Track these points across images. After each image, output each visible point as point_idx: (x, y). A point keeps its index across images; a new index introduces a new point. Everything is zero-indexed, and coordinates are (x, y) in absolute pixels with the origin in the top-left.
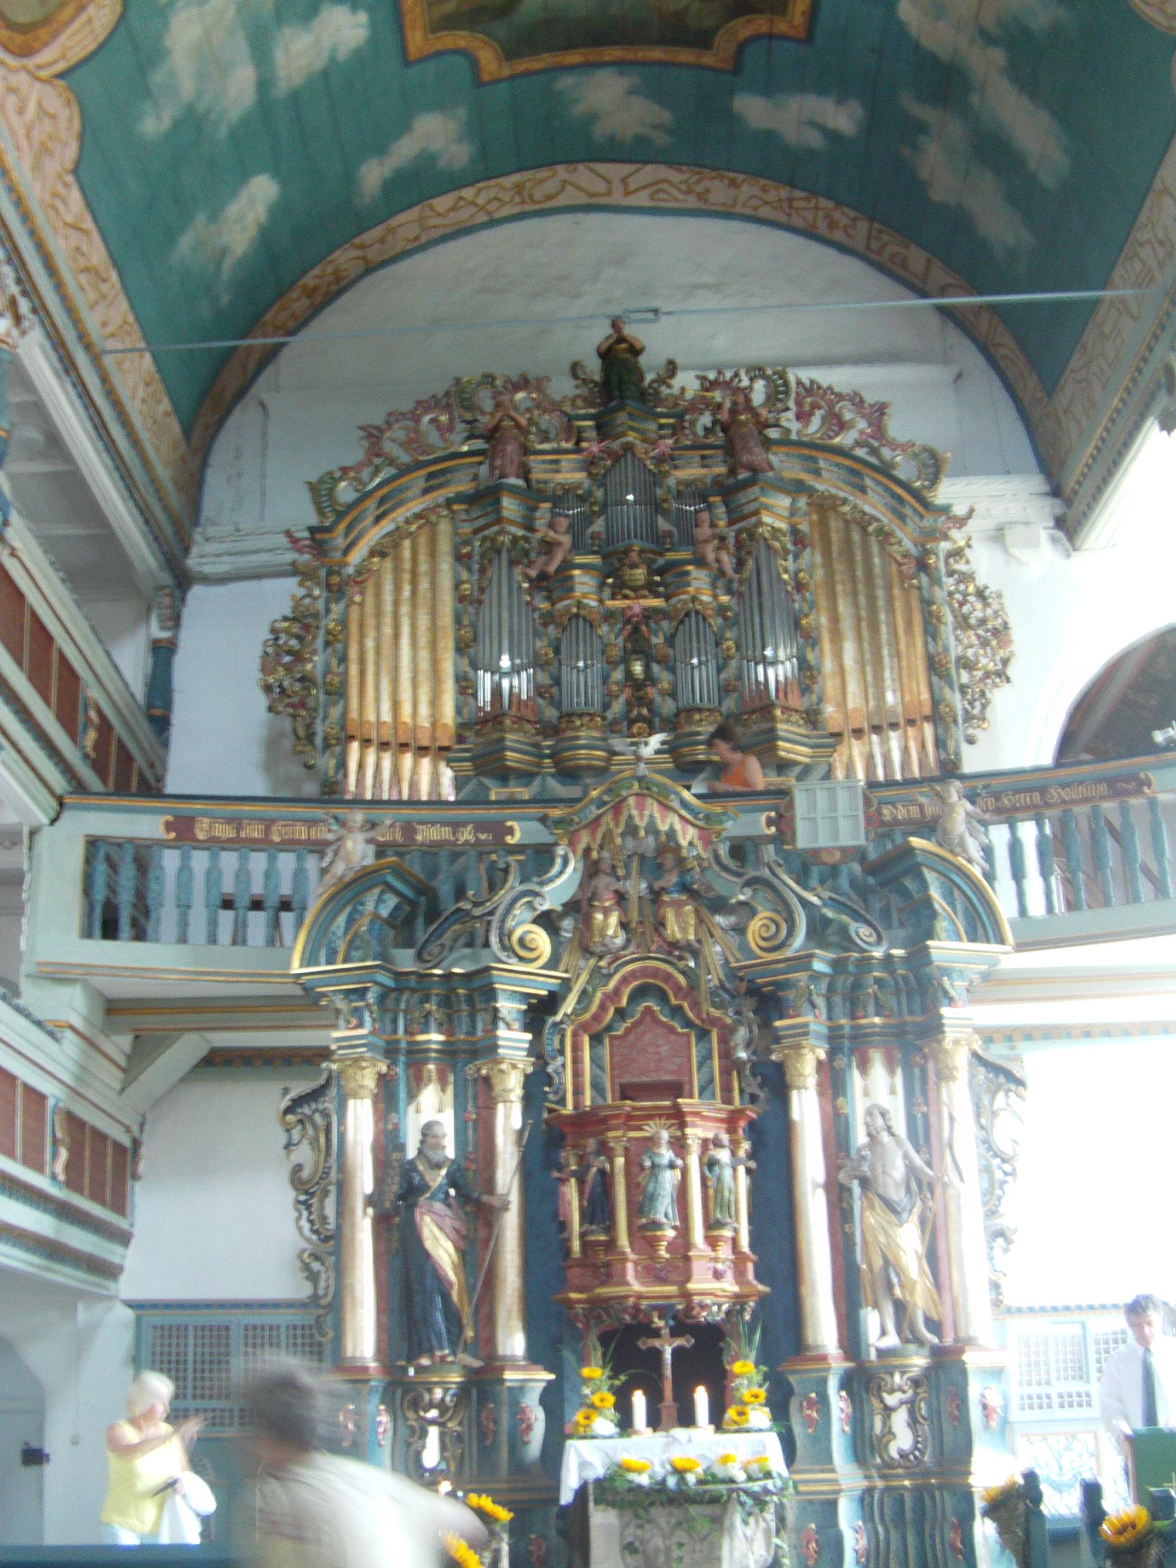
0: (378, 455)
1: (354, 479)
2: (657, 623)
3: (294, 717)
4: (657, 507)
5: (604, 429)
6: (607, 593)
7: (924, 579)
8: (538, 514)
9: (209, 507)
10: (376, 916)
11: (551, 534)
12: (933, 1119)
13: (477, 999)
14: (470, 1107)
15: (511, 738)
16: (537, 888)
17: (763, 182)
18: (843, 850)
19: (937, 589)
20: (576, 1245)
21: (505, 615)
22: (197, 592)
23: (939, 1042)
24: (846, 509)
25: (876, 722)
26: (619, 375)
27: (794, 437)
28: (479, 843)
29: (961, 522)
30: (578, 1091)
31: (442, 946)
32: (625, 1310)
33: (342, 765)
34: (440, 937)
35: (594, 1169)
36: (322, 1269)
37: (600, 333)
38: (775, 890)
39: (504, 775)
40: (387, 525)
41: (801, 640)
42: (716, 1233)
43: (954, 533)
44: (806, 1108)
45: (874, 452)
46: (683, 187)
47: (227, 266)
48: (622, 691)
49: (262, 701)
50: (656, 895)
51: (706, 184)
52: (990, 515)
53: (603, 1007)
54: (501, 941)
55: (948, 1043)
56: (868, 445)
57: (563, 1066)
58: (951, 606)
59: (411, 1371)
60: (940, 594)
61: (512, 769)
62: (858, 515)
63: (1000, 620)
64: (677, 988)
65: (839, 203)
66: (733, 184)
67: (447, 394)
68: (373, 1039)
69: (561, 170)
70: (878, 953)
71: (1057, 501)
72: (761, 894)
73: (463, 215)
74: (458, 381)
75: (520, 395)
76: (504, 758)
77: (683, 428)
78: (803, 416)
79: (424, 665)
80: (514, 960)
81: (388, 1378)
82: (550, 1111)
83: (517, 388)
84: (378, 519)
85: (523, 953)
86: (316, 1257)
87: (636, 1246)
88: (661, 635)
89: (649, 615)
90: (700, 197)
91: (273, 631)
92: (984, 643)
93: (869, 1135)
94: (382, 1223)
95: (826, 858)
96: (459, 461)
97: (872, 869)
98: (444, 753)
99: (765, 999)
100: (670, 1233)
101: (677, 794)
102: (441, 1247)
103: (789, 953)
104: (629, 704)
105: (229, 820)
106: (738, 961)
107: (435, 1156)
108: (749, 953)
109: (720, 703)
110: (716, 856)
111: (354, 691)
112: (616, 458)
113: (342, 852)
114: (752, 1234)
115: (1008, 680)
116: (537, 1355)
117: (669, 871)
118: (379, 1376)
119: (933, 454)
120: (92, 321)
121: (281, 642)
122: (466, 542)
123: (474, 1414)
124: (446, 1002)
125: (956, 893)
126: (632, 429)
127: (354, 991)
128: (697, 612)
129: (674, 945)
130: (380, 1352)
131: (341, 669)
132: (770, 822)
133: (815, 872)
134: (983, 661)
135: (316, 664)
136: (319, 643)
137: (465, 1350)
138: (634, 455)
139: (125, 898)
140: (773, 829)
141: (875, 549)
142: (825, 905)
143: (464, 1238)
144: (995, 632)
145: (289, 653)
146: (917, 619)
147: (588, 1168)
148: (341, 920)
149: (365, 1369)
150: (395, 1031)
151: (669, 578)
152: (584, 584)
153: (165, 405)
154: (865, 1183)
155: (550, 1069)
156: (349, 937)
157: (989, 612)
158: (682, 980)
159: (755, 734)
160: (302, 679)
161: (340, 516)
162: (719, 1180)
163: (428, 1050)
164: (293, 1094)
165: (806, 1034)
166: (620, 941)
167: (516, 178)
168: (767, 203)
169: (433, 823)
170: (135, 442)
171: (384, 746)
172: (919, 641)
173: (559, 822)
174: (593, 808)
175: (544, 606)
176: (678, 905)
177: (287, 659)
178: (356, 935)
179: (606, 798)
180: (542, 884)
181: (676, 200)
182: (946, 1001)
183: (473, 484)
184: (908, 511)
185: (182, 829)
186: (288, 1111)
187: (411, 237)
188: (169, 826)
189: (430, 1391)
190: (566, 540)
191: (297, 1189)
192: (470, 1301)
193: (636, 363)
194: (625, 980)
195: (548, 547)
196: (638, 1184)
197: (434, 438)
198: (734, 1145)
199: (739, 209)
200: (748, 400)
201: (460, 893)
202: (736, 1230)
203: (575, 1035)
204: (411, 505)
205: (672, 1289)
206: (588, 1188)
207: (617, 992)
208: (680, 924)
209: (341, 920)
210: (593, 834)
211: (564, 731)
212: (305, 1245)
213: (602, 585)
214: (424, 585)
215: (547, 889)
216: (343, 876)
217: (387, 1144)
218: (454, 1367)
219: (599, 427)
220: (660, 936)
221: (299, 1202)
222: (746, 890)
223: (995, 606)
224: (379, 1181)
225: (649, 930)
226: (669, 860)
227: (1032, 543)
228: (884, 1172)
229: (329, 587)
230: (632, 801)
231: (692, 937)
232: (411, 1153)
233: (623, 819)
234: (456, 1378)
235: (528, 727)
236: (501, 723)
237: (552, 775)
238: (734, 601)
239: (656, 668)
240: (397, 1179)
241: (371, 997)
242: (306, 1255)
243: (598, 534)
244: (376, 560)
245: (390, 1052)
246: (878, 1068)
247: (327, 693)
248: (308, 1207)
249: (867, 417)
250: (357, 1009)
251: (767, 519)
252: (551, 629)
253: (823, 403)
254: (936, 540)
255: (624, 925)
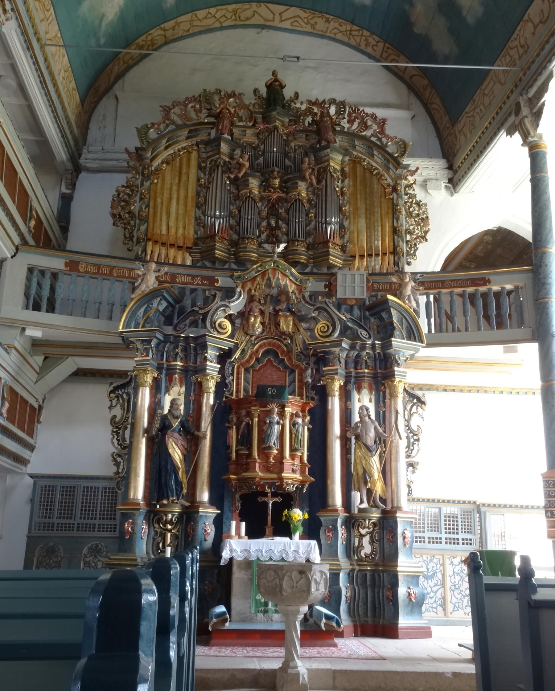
0: (168, 120)
5: (266, 119)
9: (90, 138)
10: (157, 310)
11: (241, 160)
12: (387, 414)
13: (198, 349)
14: (192, 394)
17: (341, 20)
18: (356, 299)
19: (400, 200)
20: (234, 455)
21: (218, 194)
22: (83, 175)
23: (393, 381)
26: (274, 95)
27: (346, 130)
29: (413, 173)
30: (238, 391)
32: (254, 484)
34: (184, 321)
35: (244, 423)
36: (122, 461)
37: (269, 77)
40: (170, 151)
41: (341, 216)
42: (294, 453)
43: (410, 178)
44: (335, 405)
45: (380, 139)
46: (306, 20)
47: (104, 24)
48: (265, 231)
49: (111, 220)
51: (316, 19)
52: (424, 172)
53: (251, 357)
54: (211, 324)
55: (396, 383)
56: (378, 137)
57: (233, 380)
58: (405, 208)
59: (158, 506)
60: (401, 202)
61: (217, 258)
63: (425, 216)
64: (283, 352)
65: (372, 33)
66: (328, 21)
68: (152, 362)
69: (254, 4)
71: (451, 171)
73: (210, 22)
74: (205, 90)
75: (231, 100)
76: (215, 253)
78: (351, 122)
80: (216, 333)
81: (148, 509)
82: (226, 397)
84: (166, 148)
85: (220, 330)
86: (119, 456)
87: (260, 456)
88: (283, 209)
90: (313, 26)
91: (117, 191)
92: (418, 224)
93: (360, 417)
94: (151, 442)
95: (349, 302)
96: (203, 126)
97: (369, 308)
99: (321, 359)
100: (276, 452)
102: (176, 453)
103: (332, 339)
104: (268, 235)
106: (309, 341)
107: (176, 413)
108: (315, 338)
109: (306, 240)
110: (304, 298)
111: (151, 220)
114: (308, 456)
115: (426, 240)
116: (213, 502)
117: (283, 302)
118: (145, 508)
119: (404, 143)
120: (42, 28)
121: (120, 196)
123: (184, 527)
124: (185, 349)
125: (404, 320)
126: (278, 119)
127: (145, 341)
128: (300, 200)
129: (284, 333)
130: (145, 497)
133: (344, 307)
134: (417, 232)
135: (135, 207)
137: (183, 498)
139: (46, 293)
142: (348, 321)
143: (186, 449)
144: (423, 219)
145: (123, 201)
147: (241, 422)
148: (142, 310)
149: (139, 504)
150: (162, 360)
152: (254, 183)
153: (73, 85)
154: (358, 438)
155: (227, 381)
156: (144, 318)
158: (285, 349)
160: (129, 213)
162: (297, 431)
163: (176, 369)
164: (115, 385)
165: (337, 374)
167: (234, 6)
168: (341, 32)
169: (184, 275)
170: (57, 91)
171: (163, 244)
177: (123, 204)
178: (148, 317)
180: (229, 302)
181: (302, 27)
182: (396, 365)
185: (72, 266)
186: (111, 392)
187: (186, 29)
188: (66, 265)
189: (166, 515)
190: (247, 164)
191: (113, 426)
192: (186, 478)
194: (261, 346)
196: (263, 430)
197: (193, 115)
198: (304, 417)
199: (328, 34)
200: (328, 113)
201: (194, 304)
202: (303, 453)
203: (238, 368)
205: (274, 476)
206: (241, 431)
207: (257, 351)
208: (287, 324)
209: (142, 310)
210: (253, 284)
212: (116, 451)
215: (232, 305)
216: (144, 291)
217: (155, 406)
218: (177, 505)
220: (277, 329)
221: (113, 431)
222: (315, 312)
224: (150, 422)
226: (283, 298)
227: (438, 188)
228: (366, 434)
229: (143, 174)
232: (166, 411)
233: (266, 277)
234: (177, 510)
236: (215, 238)
237: (234, 263)
238: (315, 198)
240: (159, 422)
241: (153, 344)
242: (115, 455)
245: (159, 368)
246: (365, 392)
248: (117, 434)
249: (378, 124)
250: (146, 348)
251: (332, 164)
252: (237, 202)
253: (359, 117)
254: (401, 179)
255: (263, 324)
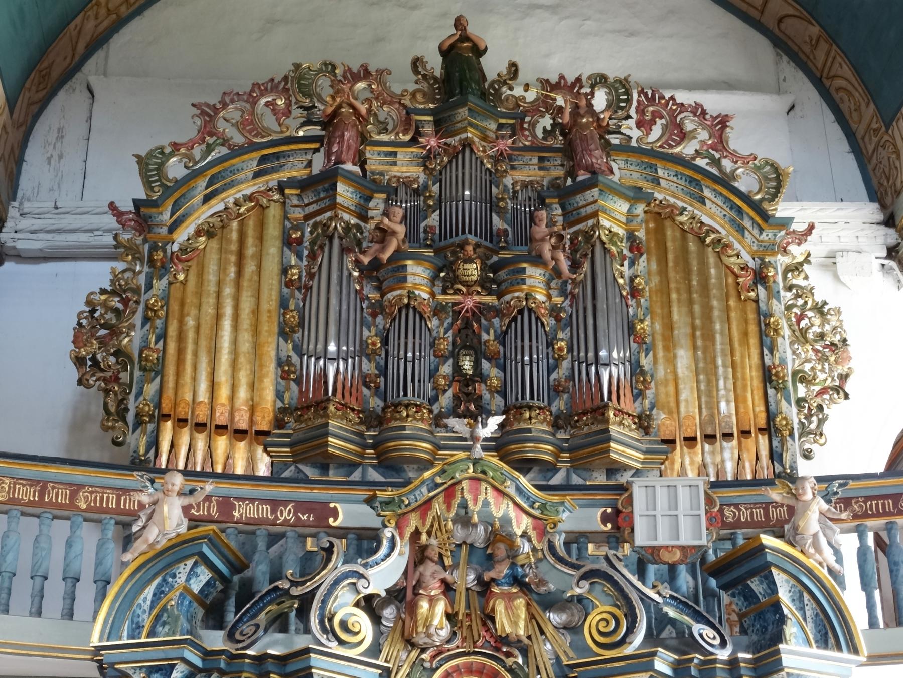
0: (211, 134)
1: (185, 156)
2: (489, 320)
3: (107, 392)
4: (493, 205)
5: (442, 126)
6: (438, 289)
7: (761, 290)
8: (372, 204)
9: (25, 184)
10: (187, 590)
11: (386, 221)
15: (334, 425)
16: (361, 570)
18: (683, 548)
19: (774, 301)
21: (334, 301)
24: (683, 219)
25: (709, 431)
26: (460, 71)
27: (634, 143)
28: (298, 523)
31: (258, 626)
33: (155, 443)
34: (255, 616)
37: (448, 31)
38: (615, 584)
39: (324, 462)
40: (216, 206)
41: (634, 346)
45: (716, 163)
48: (450, 386)
49: (73, 373)
50: (485, 587)
54: (321, 623)
60: (778, 308)
61: (332, 456)
62: (696, 226)
63: (838, 337)
67: (286, 78)
70: (724, 655)
71: (891, 231)
72: (598, 588)
74: (297, 66)
75: (361, 85)
76: (326, 444)
77: (523, 129)
79: (245, 346)
83: (356, 78)
84: (207, 199)
88: (492, 332)
89: (481, 310)
91: (89, 302)
92: (823, 359)
96: (293, 147)
97: (718, 570)
98: (261, 438)
101: (514, 479)
103: (629, 650)
105: (33, 482)
106: (570, 659)
108: (588, 651)
111: (170, 370)
112: (455, 155)
113: (156, 517)
115: (847, 397)
122: (296, 228)
125: (806, 596)
126: (471, 125)
128: (530, 310)
129: (504, 640)
131: (160, 345)
132: (605, 519)
134: (821, 376)
136: (138, 319)
138: (472, 151)
140: (609, 525)
141: (712, 259)
145: (103, 326)
146: (753, 328)
151: (502, 274)
152: (418, 274)
156: (155, 612)
157: (827, 328)
159: (588, 435)
160: (117, 354)
161: (167, 191)
166: (445, 633)
169: (252, 500)
172: (755, 352)
173: (387, 503)
174: (424, 489)
175: (374, 295)
176: (510, 598)
177: (103, 332)
178: (164, 609)
179: (439, 480)
183: (307, 171)
184: (747, 223)
190: (401, 230)
193: (479, 63)
195: (384, 234)
197: (269, 121)
200: (590, 105)
204: (242, 187)
210: (423, 517)
211: (390, 420)
213: (434, 279)
214: (250, 267)
215: (370, 573)
219: (438, 123)
222: (583, 583)
223: (834, 323)
225: (476, 625)
226: (501, 550)
229: (151, 262)
230: (465, 484)
231: (521, 632)
235: (352, 415)
239: (485, 365)
243: (432, 227)
244: (203, 239)
247: (143, 369)
251: (605, 223)
252: (380, 319)
254: (774, 253)
